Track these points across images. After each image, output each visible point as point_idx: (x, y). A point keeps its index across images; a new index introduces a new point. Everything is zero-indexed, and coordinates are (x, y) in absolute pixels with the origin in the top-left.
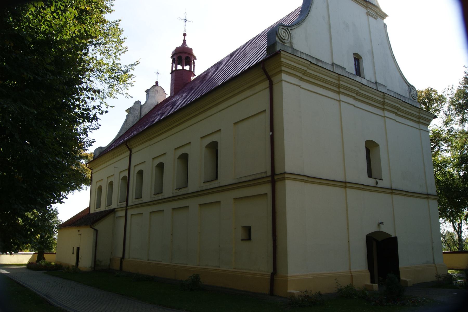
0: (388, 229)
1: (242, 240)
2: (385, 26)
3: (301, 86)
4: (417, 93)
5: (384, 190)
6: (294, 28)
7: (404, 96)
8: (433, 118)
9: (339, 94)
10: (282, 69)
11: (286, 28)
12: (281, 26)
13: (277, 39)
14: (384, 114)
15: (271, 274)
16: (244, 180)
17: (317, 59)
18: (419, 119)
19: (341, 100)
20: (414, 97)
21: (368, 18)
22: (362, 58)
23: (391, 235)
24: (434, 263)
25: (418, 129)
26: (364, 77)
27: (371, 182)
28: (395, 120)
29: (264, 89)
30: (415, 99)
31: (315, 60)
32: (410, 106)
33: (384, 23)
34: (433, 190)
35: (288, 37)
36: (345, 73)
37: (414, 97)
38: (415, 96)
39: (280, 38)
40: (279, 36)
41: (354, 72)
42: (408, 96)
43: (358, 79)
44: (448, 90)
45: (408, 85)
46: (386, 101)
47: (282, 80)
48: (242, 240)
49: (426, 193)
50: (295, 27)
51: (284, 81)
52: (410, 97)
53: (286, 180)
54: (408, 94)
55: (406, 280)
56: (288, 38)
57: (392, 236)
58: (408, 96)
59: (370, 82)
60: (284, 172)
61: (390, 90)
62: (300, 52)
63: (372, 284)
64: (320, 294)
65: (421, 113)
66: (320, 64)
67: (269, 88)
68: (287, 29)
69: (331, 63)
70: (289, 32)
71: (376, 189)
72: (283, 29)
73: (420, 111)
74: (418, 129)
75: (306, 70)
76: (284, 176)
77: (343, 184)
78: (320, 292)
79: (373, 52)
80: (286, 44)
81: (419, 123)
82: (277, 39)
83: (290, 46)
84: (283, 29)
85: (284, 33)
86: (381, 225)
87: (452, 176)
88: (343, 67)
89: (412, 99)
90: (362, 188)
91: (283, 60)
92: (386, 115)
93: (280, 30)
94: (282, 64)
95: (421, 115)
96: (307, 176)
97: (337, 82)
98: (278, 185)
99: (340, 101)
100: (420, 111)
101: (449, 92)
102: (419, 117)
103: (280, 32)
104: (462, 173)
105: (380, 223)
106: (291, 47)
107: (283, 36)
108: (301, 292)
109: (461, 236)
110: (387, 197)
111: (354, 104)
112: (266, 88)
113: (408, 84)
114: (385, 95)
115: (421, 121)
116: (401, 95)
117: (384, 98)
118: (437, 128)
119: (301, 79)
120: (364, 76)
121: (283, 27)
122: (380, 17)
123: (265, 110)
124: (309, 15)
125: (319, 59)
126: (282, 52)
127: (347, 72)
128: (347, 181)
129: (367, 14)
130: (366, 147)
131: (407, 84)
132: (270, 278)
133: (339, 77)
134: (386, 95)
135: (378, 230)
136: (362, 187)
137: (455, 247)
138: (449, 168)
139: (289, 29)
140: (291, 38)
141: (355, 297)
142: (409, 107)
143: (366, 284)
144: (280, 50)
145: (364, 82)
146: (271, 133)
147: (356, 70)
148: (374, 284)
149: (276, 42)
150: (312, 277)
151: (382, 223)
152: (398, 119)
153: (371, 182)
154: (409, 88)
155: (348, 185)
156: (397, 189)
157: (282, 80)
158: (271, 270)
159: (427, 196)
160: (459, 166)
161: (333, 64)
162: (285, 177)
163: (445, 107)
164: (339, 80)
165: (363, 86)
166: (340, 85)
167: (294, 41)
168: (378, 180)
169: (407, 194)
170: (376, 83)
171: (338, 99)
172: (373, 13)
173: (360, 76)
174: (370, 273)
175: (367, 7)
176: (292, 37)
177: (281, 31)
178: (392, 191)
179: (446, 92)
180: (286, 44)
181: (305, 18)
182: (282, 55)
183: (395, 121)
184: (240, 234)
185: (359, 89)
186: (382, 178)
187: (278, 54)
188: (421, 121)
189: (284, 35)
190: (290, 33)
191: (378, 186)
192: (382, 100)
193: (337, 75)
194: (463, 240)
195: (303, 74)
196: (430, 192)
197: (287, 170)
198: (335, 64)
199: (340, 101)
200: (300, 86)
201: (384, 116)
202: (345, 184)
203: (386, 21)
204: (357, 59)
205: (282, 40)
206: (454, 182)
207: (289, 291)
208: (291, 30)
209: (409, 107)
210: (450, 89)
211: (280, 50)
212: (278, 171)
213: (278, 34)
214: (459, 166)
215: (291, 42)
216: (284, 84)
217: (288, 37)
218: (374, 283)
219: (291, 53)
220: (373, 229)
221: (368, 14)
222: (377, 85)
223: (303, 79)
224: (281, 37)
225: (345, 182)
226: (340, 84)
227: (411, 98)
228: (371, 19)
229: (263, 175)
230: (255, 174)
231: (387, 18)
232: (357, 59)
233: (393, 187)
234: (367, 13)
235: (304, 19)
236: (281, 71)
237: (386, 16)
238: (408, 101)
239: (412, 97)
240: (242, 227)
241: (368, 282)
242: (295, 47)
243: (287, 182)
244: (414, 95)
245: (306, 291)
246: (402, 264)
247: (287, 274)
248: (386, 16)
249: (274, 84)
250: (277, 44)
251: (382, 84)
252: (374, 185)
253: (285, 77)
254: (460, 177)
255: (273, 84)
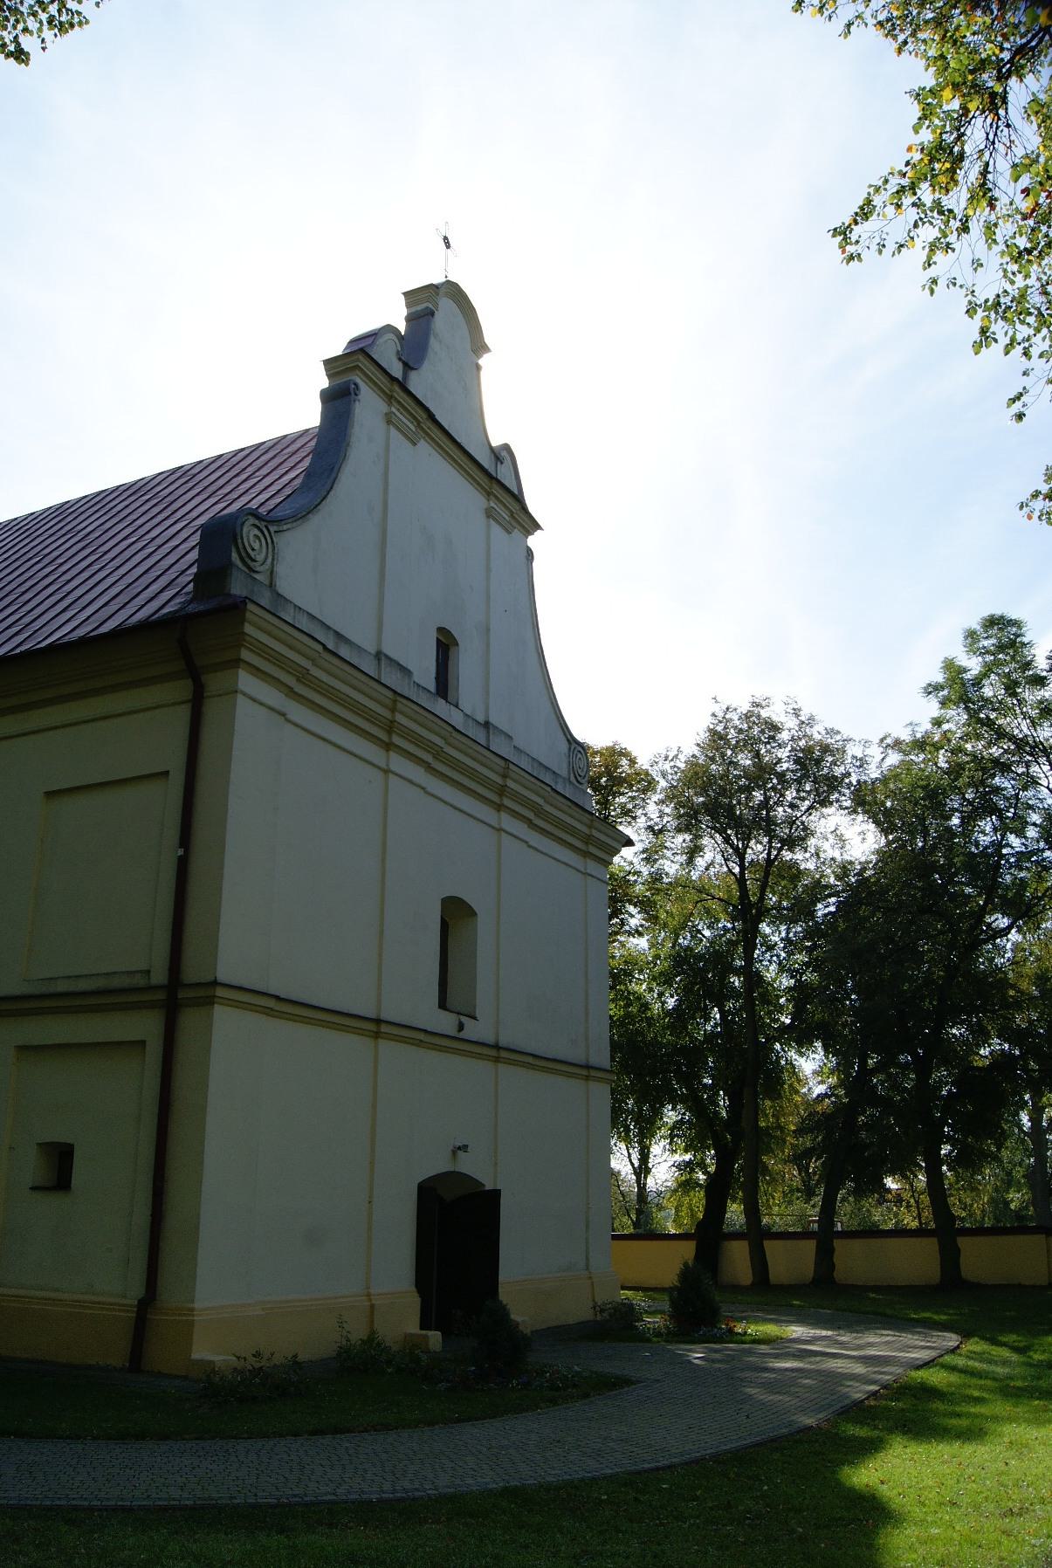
0: (476, 1167)
1: (33, 1189)
2: (529, 554)
3: (288, 716)
4: (588, 767)
5: (478, 1049)
6: (285, 527)
7: (554, 772)
8: (624, 846)
9: (387, 751)
10: (242, 657)
11: (262, 525)
12: (250, 517)
13: (234, 556)
14: (499, 818)
15: (139, 1301)
16: (61, 987)
17: (338, 635)
18: (587, 843)
19: (393, 768)
20: (580, 776)
21: (489, 526)
22: (457, 645)
23: (484, 1185)
24: (587, 1268)
25: (581, 872)
26: (458, 703)
27: (445, 1022)
28: (526, 842)
29: (174, 704)
30: (581, 784)
31: (331, 635)
32: (570, 804)
33: (528, 547)
34: (601, 1055)
35: (267, 553)
36: (409, 684)
37: (580, 776)
38: (582, 774)
39: (244, 554)
40: (240, 546)
41: (432, 687)
42: (564, 772)
43: (440, 707)
44: (665, 760)
45: (568, 740)
46: (510, 783)
47: (236, 692)
48: (33, 1189)
49: (583, 1062)
50: (289, 526)
51: (244, 694)
52: (569, 774)
53: (216, 1005)
54: (565, 765)
55: (849, 1326)
56: (266, 558)
57: (487, 1188)
58: (564, 772)
59: (470, 722)
60: (210, 978)
61: (521, 751)
62: (295, 606)
63: (424, 1332)
64: (295, 1364)
65: (596, 829)
66: (344, 652)
67: (190, 705)
68: (266, 527)
69: (372, 649)
70: (272, 539)
71: (456, 1043)
72: (254, 525)
73: (592, 821)
74: (581, 872)
75: (308, 668)
76: (209, 992)
77: (372, 1027)
78: (295, 1356)
79: (488, 630)
80: (256, 576)
81: (585, 857)
82: (234, 556)
83: (267, 582)
84: (254, 525)
85: (257, 541)
86: (460, 1153)
87: (645, 1007)
88: (405, 665)
89: (576, 783)
90: (421, 1041)
91: (248, 629)
92: (504, 826)
93: (245, 530)
94: (244, 640)
95: (594, 833)
96: (277, 998)
97: (388, 714)
98: (189, 1020)
99: (387, 771)
100: (592, 821)
101: (667, 766)
102: (588, 839)
103: (244, 535)
104: (671, 1003)
105: (459, 1148)
106: (271, 585)
107: (253, 550)
108: (238, 1358)
109: (645, 1184)
110: (481, 1069)
111: (424, 785)
112: (183, 703)
113: (569, 737)
114: (508, 768)
115: (593, 850)
116: (547, 768)
117: (505, 776)
118: (622, 863)
119: (291, 693)
120: (458, 699)
121: (257, 522)
122: (519, 528)
123: (166, 773)
124: (332, 493)
125: (342, 632)
126: (250, 606)
127: (414, 682)
128: (384, 1016)
129: (486, 513)
130: (442, 918)
131: (565, 734)
132: (134, 1315)
133: (395, 701)
134: (511, 766)
135: (452, 1170)
136: (422, 1036)
137: (625, 1219)
138: (640, 986)
139: (272, 529)
140: (273, 559)
141: (389, 1370)
142: (565, 808)
143: (408, 1331)
144: (247, 601)
145: (456, 718)
146: (181, 852)
147: (437, 678)
148: (430, 1333)
149: (231, 564)
150: (263, 1313)
151: (464, 1148)
152: (535, 839)
153: (445, 1022)
154: (570, 749)
155: (384, 1028)
156: (512, 1047)
157: (236, 692)
158: (136, 1291)
159: (586, 1070)
160: (665, 979)
161: (379, 655)
162: (215, 996)
163: (654, 809)
164: (393, 710)
165: (453, 735)
166: (396, 724)
167: (280, 569)
168: (464, 1019)
169: (538, 1062)
170: (487, 725)
171: (383, 765)
172: (503, 514)
173: (445, 697)
174: (419, 1299)
175: (489, 494)
176: (276, 557)
177: (249, 533)
178: (497, 1052)
179: (660, 765)
180: (256, 576)
181: (319, 500)
182: (248, 615)
183: (525, 845)
184: (32, 1167)
185: (443, 742)
186: (475, 1012)
187: (237, 608)
188: (593, 850)
189: (256, 546)
190: (272, 542)
191: (461, 1035)
192: (499, 780)
193: (389, 694)
194: (649, 1199)
195: (298, 680)
196: (594, 1061)
197: (223, 975)
198: (387, 657)
199: (387, 771)
200: (283, 715)
201: (497, 826)
202: (376, 1027)
203: (533, 541)
204: (446, 645)
205: (247, 559)
206: (650, 1025)
207: (195, 1356)
208: (275, 532)
209: (565, 808)
210: (670, 758)
211: (247, 601)
212: (191, 973)
213: (239, 541)
214: (665, 979)
215: (272, 573)
216: (243, 706)
217: (267, 553)
218: (431, 1330)
219: (270, 610)
220: (438, 1165)
221: (489, 514)
222: (488, 732)
223: (296, 693)
224: (247, 552)
225: (378, 1021)
226: (395, 721)
227: (572, 779)
228: (496, 530)
229: (140, 981)
230: (107, 974)
231: (538, 532)
232: (446, 645)
233: (503, 1042)
234: (486, 509)
235: (316, 503)
236: (236, 663)
237: (537, 526)
238: (564, 788)
239: (574, 774)
240: (39, 1144)
241: (412, 1326)
242: (283, 587)
243: (219, 1012)
244: (579, 771)
245: (257, 1355)
246: (508, 1271)
247: (193, 1302)
248: (537, 526)
249: (209, 697)
250: (235, 572)
251: (501, 730)
252: (452, 1032)
253: (246, 680)
254: (668, 1013)
255: (205, 695)
